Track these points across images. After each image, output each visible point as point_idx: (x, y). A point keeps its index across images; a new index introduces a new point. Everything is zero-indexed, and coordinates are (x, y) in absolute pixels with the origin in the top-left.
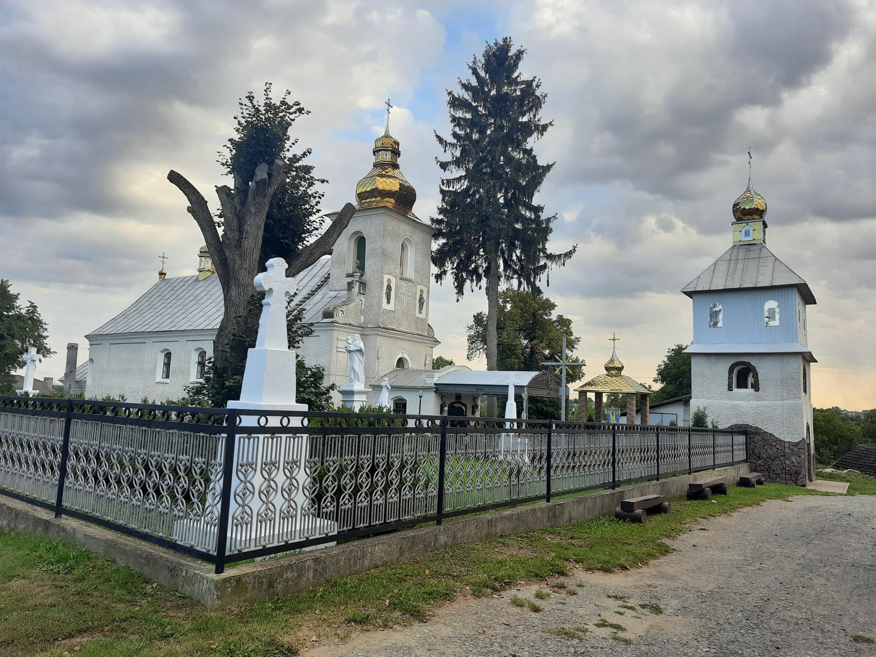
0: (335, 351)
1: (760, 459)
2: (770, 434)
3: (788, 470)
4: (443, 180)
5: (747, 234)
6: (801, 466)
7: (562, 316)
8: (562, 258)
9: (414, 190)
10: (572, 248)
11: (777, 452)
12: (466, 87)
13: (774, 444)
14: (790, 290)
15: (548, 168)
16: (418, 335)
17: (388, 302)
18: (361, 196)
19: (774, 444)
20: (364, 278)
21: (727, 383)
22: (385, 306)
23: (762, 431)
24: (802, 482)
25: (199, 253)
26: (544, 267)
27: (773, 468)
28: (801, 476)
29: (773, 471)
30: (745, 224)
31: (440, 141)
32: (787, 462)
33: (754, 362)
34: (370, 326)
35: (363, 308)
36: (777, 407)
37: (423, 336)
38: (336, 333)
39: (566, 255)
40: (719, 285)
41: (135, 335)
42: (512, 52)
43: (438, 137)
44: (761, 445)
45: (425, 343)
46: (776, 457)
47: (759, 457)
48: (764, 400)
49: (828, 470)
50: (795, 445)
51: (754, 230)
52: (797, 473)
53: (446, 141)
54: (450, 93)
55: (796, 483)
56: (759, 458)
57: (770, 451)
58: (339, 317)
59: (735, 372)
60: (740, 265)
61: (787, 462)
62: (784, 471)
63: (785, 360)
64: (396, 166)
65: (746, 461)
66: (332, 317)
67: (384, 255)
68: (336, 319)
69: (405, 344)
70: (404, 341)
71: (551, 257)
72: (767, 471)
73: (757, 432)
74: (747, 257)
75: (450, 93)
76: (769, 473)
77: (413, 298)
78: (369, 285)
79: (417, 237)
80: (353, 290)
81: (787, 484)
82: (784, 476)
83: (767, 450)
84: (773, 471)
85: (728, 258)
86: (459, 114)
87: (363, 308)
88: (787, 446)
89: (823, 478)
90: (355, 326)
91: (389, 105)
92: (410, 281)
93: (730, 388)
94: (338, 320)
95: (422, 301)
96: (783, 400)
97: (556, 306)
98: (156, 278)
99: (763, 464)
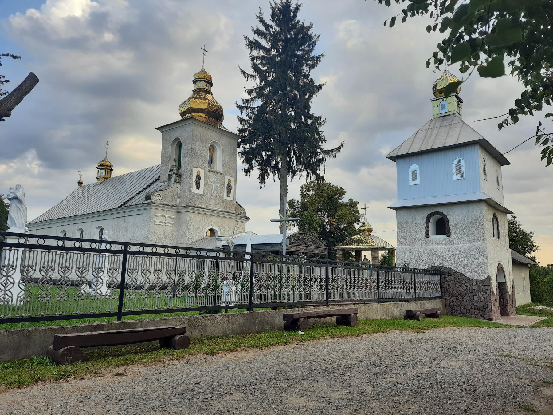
0: (153, 224)
1: (453, 296)
2: (461, 273)
3: (476, 305)
4: (243, 100)
5: (443, 107)
6: (487, 302)
7: (352, 200)
8: (334, 152)
9: (221, 108)
10: (340, 145)
11: (466, 289)
12: (258, 32)
13: (464, 282)
14: (473, 147)
15: (320, 86)
16: (225, 212)
17: (198, 187)
18: (182, 114)
19: (464, 282)
20: (180, 171)
21: (424, 231)
22: (226, 197)
23: (454, 271)
24: (489, 316)
25: (97, 166)
26: (322, 160)
27: (464, 303)
28: (488, 310)
29: (464, 306)
30: (442, 100)
31: (243, 73)
32: (475, 298)
33: (445, 211)
34: (183, 206)
35: (179, 193)
36: (465, 249)
37: (230, 213)
38: (153, 211)
39: (336, 149)
40: (415, 149)
41: (46, 222)
42: (293, 7)
43: (242, 71)
44: (453, 284)
45: (234, 218)
46: (466, 294)
47: (452, 294)
48: (454, 244)
49: (539, 307)
50: (481, 283)
51: (449, 104)
52: (484, 308)
53: (247, 74)
54: (246, 38)
55: (484, 317)
56: (452, 295)
57: (460, 288)
58: (156, 199)
59: (431, 220)
60: (435, 131)
61: (475, 298)
62: (473, 306)
63: (471, 207)
64: (210, 93)
65: (441, 298)
66: (150, 199)
67: (193, 152)
68: (153, 200)
69: (215, 219)
70: (225, 219)
71: (327, 152)
72: (459, 306)
73: (450, 272)
74: (441, 126)
75: (246, 38)
76: (461, 308)
77: (221, 185)
78: (183, 176)
79: (223, 142)
80: (171, 180)
81: (476, 318)
82: (473, 310)
83: (458, 288)
84: (464, 306)
85: (427, 128)
86: (255, 53)
87: (179, 193)
88: (474, 284)
89: (533, 315)
90: (170, 206)
91: (204, 50)
92: (219, 173)
93: (427, 235)
94: (153, 201)
95: (230, 188)
96: (470, 243)
97: (346, 192)
98: (76, 185)
99: (455, 300)
